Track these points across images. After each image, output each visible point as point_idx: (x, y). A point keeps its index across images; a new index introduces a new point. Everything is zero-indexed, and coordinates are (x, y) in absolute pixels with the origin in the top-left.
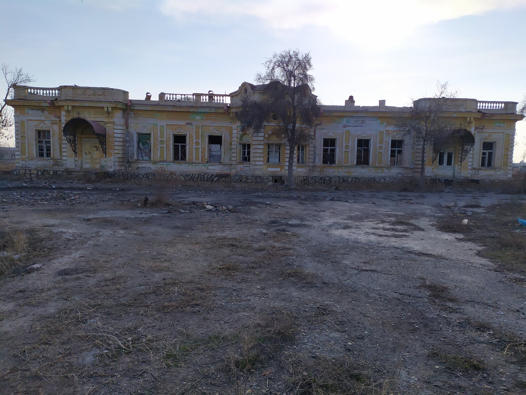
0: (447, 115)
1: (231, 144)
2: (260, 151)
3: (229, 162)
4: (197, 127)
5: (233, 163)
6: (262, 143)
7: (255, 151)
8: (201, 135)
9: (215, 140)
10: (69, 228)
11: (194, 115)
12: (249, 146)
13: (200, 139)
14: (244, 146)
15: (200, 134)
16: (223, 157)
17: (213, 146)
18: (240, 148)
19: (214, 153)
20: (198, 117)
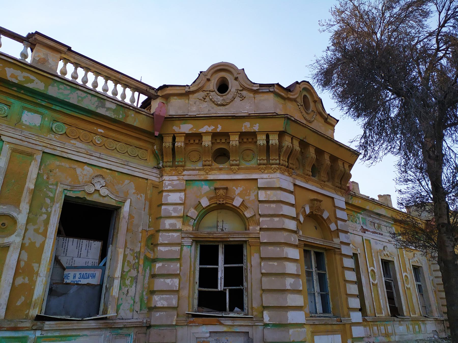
0: (111, 321)
1: (152, 242)
2: (291, 268)
3: (138, 318)
4: (21, 154)
5: (157, 318)
6: (294, 239)
7: (267, 267)
8: (34, 193)
9: (87, 220)
10: (36, 80)
11: (17, 105)
12: (235, 252)
13: (25, 207)
14: (207, 253)
15: (30, 185)
16: (115, 291)
17: (72, 244)
18: (191, 254)
19: (72, 276)
20: (31, 118)
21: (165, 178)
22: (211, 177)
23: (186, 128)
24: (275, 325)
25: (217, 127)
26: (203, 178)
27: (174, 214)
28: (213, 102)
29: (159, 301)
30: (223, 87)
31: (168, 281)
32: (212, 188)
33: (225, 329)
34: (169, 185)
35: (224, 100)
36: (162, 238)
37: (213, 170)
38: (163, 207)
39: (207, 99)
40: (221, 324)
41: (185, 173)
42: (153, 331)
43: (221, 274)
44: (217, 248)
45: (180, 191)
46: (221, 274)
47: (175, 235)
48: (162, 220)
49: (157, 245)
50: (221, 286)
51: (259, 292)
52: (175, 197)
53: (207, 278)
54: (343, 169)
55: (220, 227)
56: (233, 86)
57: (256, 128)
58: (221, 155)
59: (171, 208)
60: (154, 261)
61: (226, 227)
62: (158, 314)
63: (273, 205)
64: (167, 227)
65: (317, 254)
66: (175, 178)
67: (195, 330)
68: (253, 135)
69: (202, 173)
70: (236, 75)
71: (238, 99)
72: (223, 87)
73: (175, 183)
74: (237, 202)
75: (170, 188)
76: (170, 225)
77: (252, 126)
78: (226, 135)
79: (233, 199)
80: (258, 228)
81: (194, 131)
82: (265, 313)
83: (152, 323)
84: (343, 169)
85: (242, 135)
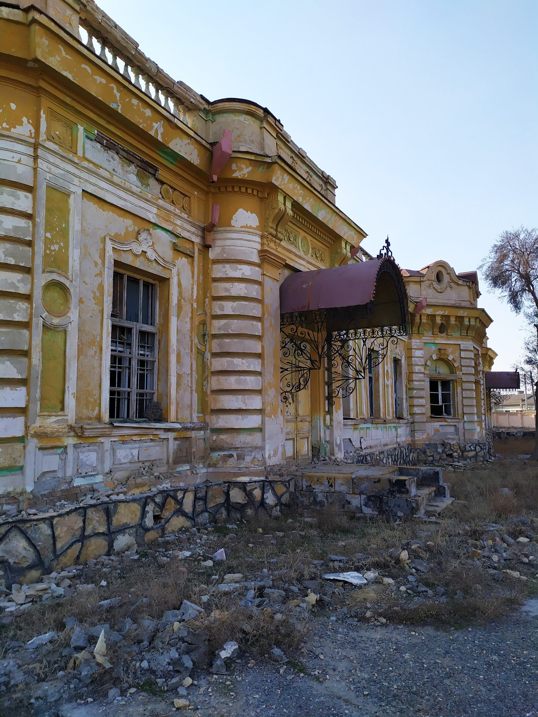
14: (433, 385)
21: (413, 340)
22: (437, 342)
23: (429, 311)
24: (468, 422)
25: (445, 312)
26: (433, 342)
27: (419, 364)
28: (435, 289)
29: (416, 410)
30: (439, 278)
31: (420, 400)
32: (437, 348)
33: (446, 424)
34: (415, 345)
35: (441, 288)
36: (415, 377)
37: (438, 337)
38: (413, 359)
39: (432, 287)
40: (446, 421)
41: (424, 338)
42: (416, 424)
43: (440, 397)
44: (437, 382)
45: (421, 349)
46: (440, 397)
47: (421, 375)
48: (414, 367)
49: (412, 381)
50: (440, 404)
51: (462, 406)
52: (418, 353)
53: (434, 398)
54: (283, 207)
55: (437, 371)
56: (446, 278)
57: (465, 314)
58: (443, 329)
59: (417, 359)
60: (413, 389)
61: (443, 371)
62: (417, 417)
63: (468, 360)
64: (417, 371)
65: (146, 285)
66: (418, 341)
67: (433, 424)
68: (462, 318)
69: (432, 338)
70: (449, 272)
71: (449, 289)
72: (439, 278)
73: (418, 344)
74: (450, 358)
75: (415, 347)
76: (419, 370)
77: (463, 313)
78: (448, 317)
79: (448, 356)
80: (461, 373)
81: (433, 313)
82: (465, 416)
83: (415, 421)
84: (283, 207)
85: (457, 317)
